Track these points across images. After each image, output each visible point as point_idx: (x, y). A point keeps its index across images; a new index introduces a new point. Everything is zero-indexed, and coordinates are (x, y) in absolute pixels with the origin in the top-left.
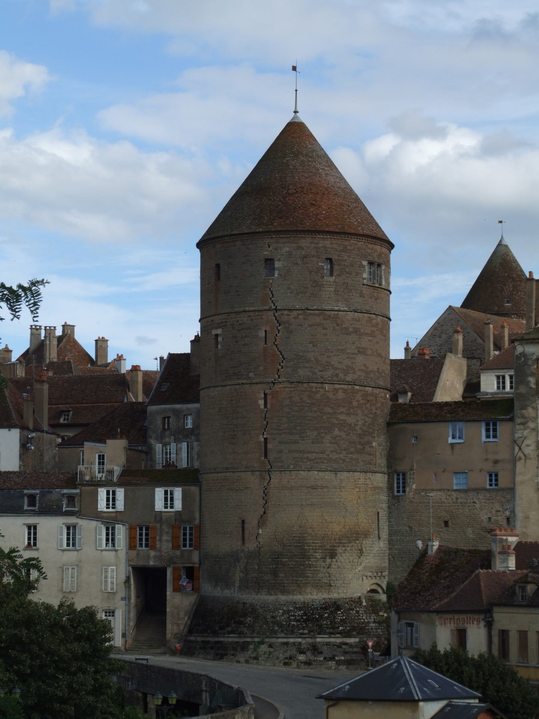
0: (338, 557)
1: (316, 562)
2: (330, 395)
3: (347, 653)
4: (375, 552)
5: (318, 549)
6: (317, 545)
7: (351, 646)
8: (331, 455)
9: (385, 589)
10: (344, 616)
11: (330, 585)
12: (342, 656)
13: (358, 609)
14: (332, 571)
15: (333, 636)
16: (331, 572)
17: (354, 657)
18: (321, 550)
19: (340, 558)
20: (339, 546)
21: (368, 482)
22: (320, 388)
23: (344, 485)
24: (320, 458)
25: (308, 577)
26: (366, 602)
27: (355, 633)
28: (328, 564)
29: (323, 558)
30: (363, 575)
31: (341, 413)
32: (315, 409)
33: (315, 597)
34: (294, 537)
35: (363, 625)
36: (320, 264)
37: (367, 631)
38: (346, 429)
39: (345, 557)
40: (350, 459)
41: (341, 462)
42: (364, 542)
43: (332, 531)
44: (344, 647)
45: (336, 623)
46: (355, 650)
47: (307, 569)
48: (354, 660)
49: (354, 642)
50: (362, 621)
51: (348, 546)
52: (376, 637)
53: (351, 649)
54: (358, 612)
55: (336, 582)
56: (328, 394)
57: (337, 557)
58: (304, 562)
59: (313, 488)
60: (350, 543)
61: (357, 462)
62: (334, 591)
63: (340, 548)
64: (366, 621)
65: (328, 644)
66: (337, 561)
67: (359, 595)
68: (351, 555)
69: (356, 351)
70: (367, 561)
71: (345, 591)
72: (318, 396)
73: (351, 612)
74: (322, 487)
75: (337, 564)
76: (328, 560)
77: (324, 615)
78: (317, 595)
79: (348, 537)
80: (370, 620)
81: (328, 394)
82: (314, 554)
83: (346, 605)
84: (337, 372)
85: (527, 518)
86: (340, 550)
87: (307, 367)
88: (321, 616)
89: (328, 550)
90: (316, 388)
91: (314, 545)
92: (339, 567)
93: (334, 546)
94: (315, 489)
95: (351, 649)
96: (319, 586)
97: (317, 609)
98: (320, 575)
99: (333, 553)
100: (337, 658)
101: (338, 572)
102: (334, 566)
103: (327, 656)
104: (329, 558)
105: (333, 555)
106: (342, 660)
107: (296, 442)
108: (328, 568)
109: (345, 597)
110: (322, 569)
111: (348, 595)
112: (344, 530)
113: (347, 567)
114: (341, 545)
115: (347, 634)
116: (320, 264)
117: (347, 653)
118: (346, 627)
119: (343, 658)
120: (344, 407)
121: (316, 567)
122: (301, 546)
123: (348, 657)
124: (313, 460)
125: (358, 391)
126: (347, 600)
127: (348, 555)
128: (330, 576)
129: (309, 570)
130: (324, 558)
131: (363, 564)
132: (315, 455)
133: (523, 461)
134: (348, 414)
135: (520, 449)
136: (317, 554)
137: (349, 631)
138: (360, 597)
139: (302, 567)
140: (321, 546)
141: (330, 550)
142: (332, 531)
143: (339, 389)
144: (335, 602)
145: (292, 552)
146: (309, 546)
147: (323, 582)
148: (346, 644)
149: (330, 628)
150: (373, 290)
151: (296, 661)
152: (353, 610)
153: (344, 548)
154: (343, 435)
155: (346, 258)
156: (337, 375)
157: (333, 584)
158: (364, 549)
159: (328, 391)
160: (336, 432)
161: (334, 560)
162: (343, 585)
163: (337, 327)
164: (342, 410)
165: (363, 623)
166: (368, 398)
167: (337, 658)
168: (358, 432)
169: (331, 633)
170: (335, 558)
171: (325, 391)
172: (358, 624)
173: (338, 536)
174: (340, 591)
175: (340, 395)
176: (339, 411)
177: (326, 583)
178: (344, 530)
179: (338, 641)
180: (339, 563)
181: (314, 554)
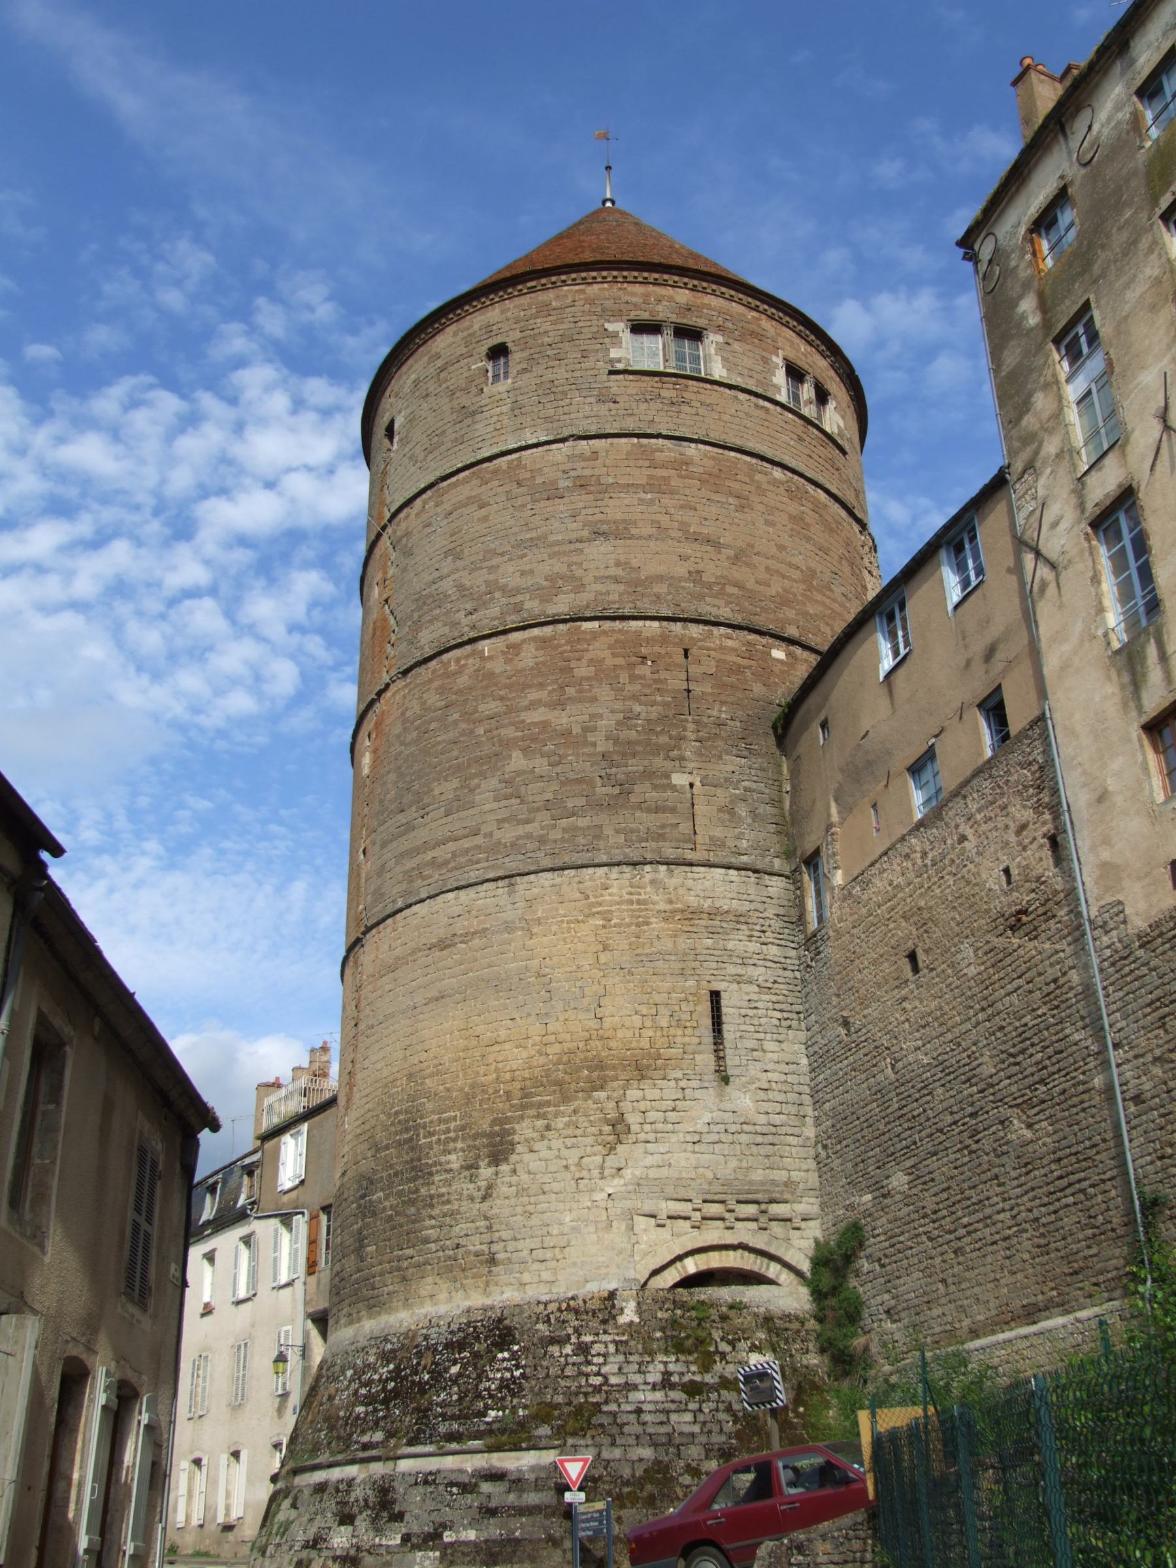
0: (521, 1155)
1: (447, 1182)
2: (497, 666)
3: (492, 1512)
4: (700, 1127)
5: (455, 1140)
6: (452, 1125)
7: (518, 1483)
8: (498, 835)
9: (808, 1274)
10: (517, 1367)
11: (492, 1261)
12: (471, 1525)
13: (588, 1338)
14: (498, 1207)
15: (454, 1446)
16: (495, 1211)
17: (519, 1528)
18: (464, 1139)
19: (527, 1157)
20: (522, 1117)
21: (648, 893)
22: (467, 657)
23: (539, 914)
24: (467, 851)
25: (426, 1241)
26: (639, 1311)
27: (544, 1430)
28: (483, 1184)
29: (468, 1167)
30: (630, 1216)
31: (533, 705)
32: (456, 716)
33: (442, 1309)
34: (396, 1113)
35: (596, 1399)
36: (473, 367)
37: (605, 1420)
38: (550, 747)
39: (545, 1154)
40: (564, 830)
41: (531, 846)
42: (633, 1094)
43: (497, 1070)
44: (486, 1487)
45: (479, 1396)
46: (532, 1498)
47: (424, 1213)
48: (517, 1541)
49: (533, 1469)
50: (597, 1381)
51: (556, 1115)
52: (655, 1445)
53: (512, 1498)
54: (583, 1349)
55: (511, 1246)
56: (489, 665)
57: (514, 1158)
58: (417, 1190)
59: (443, 945)
60: (566, 1099)
61: (598, 837)
62: (503, 1278)
63: (527, 1122)
64: (613, 1380)
65: (428, 1479)
66: (514, 1171)
67: (612, 1286)
68: (569, 1142)
69: (585, 533)
70: (650, 1160)
71: (546, 1276)
72: (463, 681)
73: (554, 1350)
74: (467, 937)
75: (514, 1179)
76: (486, 1172)
77: (447, 1370)
78: (450, 1299)
79: (560, 1083)
80: (637, 1379)
81: (489, 665)
82: (443, 1159)
83: (540, 1326)
84: (519, 598)
85: (1102, 797)
86: (525, 1129)
87: (436, 618)
88: (437, 1374)
89: (484, 1135)
90: (458, 660)
91: (443, 1127)
92: (522, 1191)
93: (508, 1120)
94: (448, 946)
95: (512, 1498)
96: (456, 1267)
97: (436, 1350)
98: (462, 1228)
99: (501, 1143)
100: (448, 1537)
101: (519, 1210)
102: (504, 1189)
103: (415, 1529)
104: (489, 1165)
105: (499, 1149)
106: (466, 1543)
107: (410, 827)
108: (484, 1198)
109: (544, 1298)
110: (465, 1204)
111: (562, 1290)
112: (542, 1060)
113: (556, 1186)
114: (531, 1112)
115: (513, 1437)
116: (473, 367)
117: (492, 1512)
118: (514, 1410)
119: (471, 1535)
120: (542, 686)
121: (448, 1202)
122: (411, 1139)
123: (494, 1530)
124: (446, 863)
125: (595, 635)
126: (552, 1307)
127: (555, 1144)
128: (489, 1228)
129: (432, 1217)
130: (472, 1166)
131: (628, 1173)
132: (451, 846)
133: (1051, 590)
134: (559, 704)
135: (1038, 554)
136: (453, 1157)
137: (522, 1425)
138: (612, 1295)
139: (413, 1210)
140: (463, 1128)
141: (491, 1135)
142: (497, 1070)
143: (524, 641)
144: (500, 1320)
145: (391, 1166)
146: (431, 1134)
147: (468, 1253)
148: (496, 1476)
149: (453, 1417)
150: (660, 385)
151: (325, 1553)
152: (562, 1341)
153: (540, 1123)
154: (540, 765)
155: (546, 327)
156: (518, 608)
157: (500, 1256)
158: (633, 1119)
159: (491, 658)
160: (517, 761)
161: (504, 1168)
162: (540, 1254)
163: (517, 491)
164: (533, 695)
165: (597, 1389)
166: (644, 651)
167: (448, 1537)
168: (599, 749)
169: (452, 1437)
170: (506, 1160)
171: (483, 658)
172: (568, 1393)
173: (517, 1085)
174: (526, 1277)
175: (529, 657)
176: (526, 703)
177: (477, 1254)
178: (542, 1060)
179: (471, 1463)
180: (525, 1177)
181: (443, 1159)
